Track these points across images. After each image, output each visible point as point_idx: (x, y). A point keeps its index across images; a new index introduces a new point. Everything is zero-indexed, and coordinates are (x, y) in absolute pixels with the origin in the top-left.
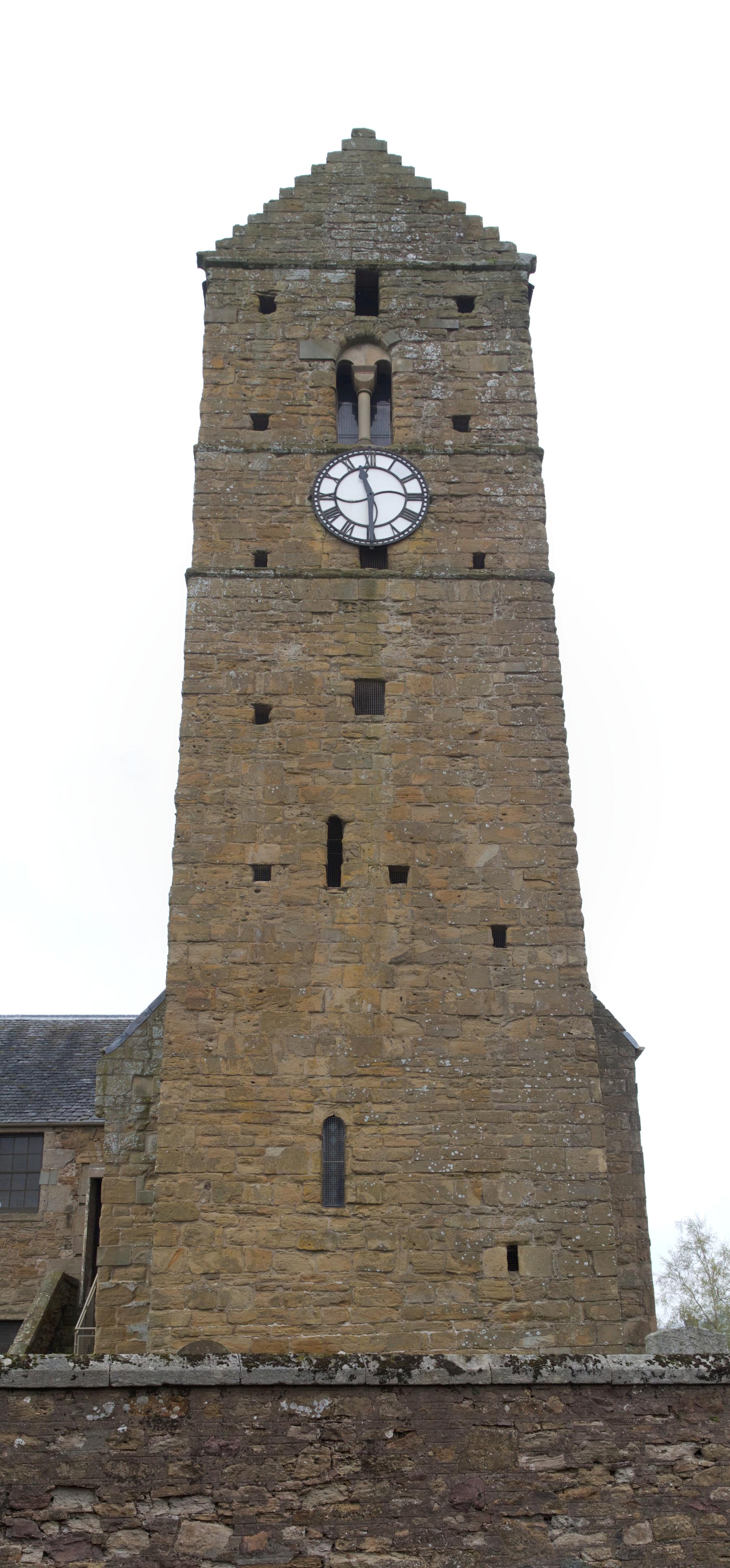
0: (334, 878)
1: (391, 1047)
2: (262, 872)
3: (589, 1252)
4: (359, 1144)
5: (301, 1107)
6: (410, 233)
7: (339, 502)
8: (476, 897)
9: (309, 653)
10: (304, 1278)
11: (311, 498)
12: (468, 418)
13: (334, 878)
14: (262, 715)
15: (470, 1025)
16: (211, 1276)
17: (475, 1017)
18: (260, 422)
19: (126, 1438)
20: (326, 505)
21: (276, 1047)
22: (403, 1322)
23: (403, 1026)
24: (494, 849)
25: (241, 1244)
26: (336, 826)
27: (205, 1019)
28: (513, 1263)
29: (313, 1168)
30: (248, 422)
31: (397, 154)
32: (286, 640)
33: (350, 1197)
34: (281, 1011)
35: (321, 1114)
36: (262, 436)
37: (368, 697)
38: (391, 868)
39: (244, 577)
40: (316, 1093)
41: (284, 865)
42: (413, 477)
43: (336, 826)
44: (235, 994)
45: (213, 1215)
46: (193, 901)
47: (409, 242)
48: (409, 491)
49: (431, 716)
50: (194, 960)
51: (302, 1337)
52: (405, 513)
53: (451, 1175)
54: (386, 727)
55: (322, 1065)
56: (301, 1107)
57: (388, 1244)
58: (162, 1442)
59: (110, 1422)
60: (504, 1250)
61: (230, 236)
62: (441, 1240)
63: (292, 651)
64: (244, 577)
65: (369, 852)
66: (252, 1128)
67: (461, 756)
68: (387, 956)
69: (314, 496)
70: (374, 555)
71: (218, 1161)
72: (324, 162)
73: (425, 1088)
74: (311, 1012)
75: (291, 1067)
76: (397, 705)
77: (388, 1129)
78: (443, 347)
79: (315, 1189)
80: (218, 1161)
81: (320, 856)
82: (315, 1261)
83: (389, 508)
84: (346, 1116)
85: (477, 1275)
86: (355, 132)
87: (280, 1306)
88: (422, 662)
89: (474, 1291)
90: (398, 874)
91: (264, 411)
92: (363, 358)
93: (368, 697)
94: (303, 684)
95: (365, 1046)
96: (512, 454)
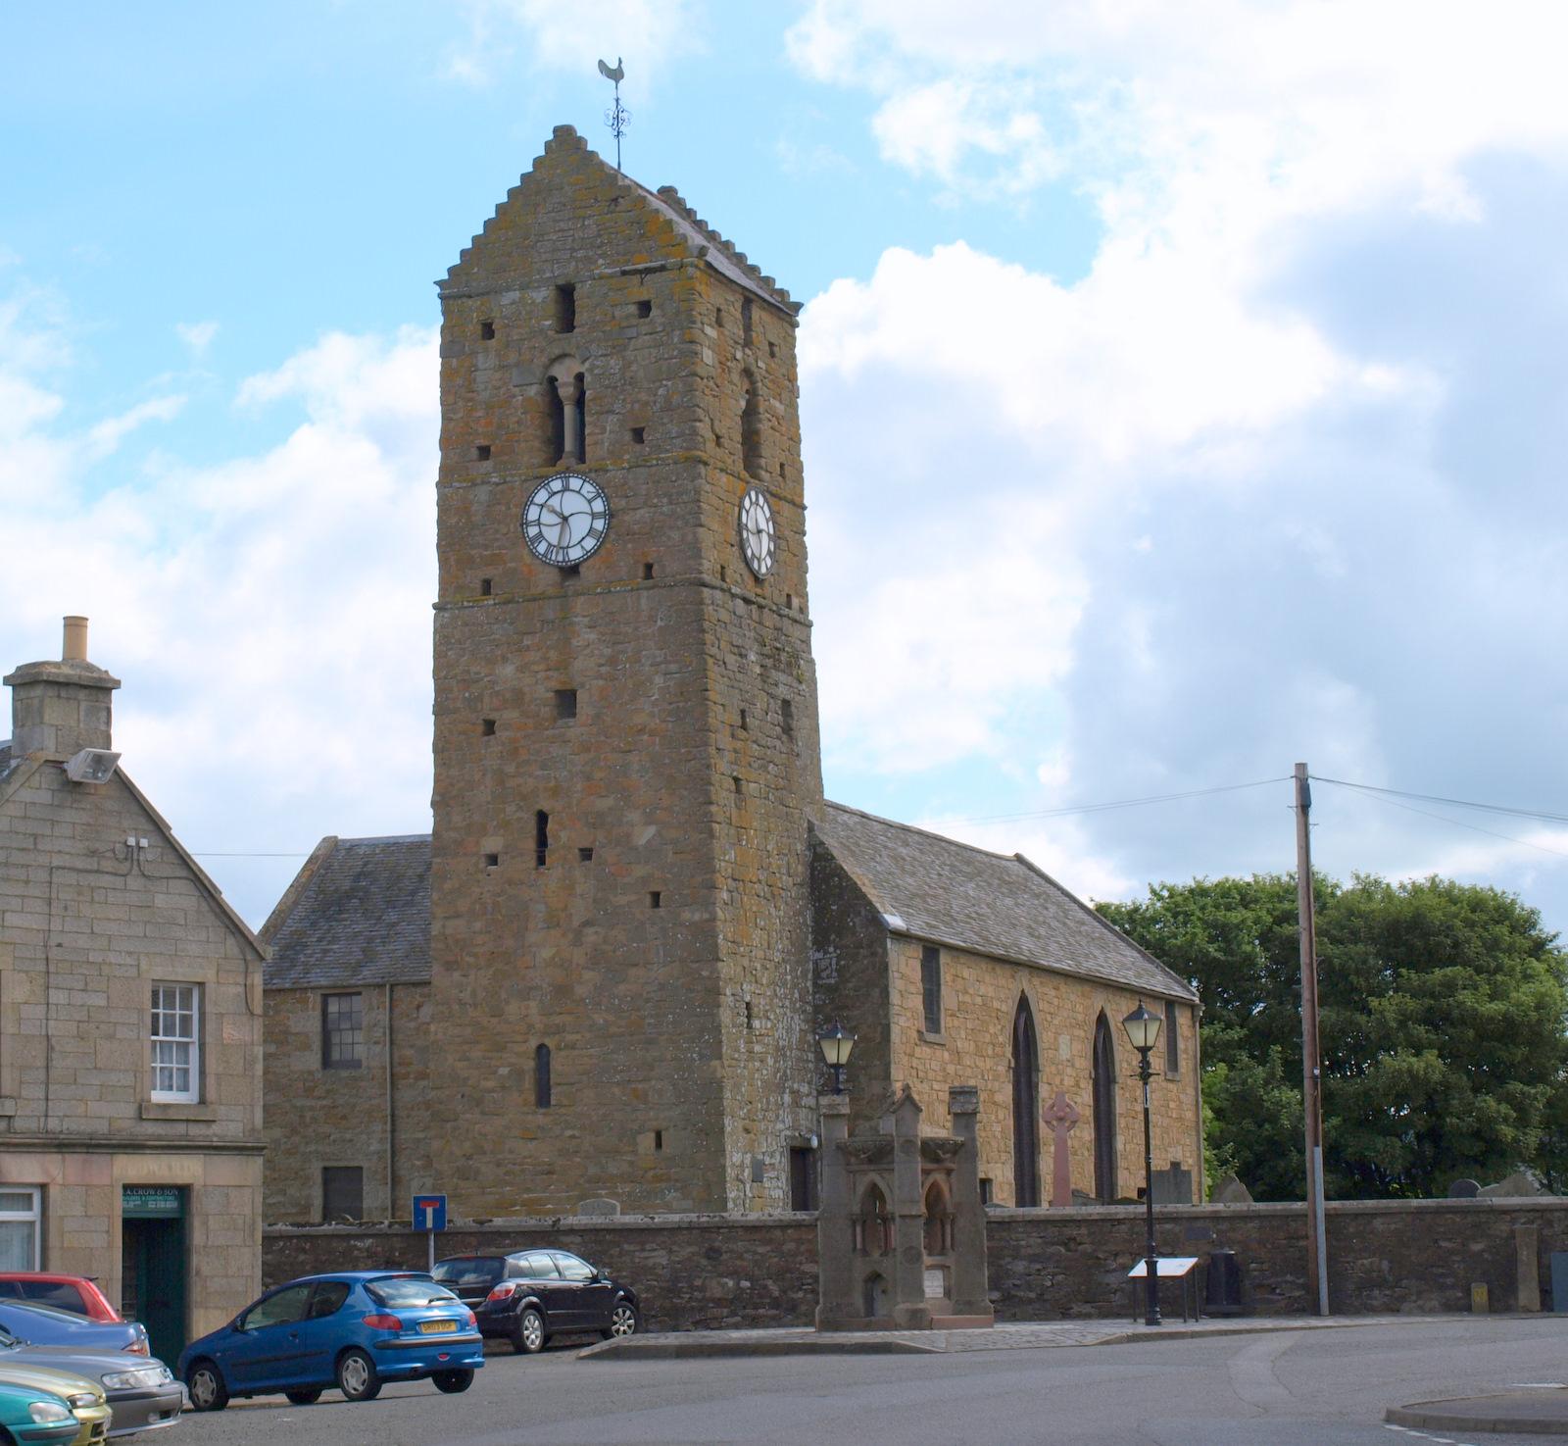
0: (541, 861)
1: (580, 991)
2: (493, 859)
3: (707, 1134)
4: (557, 1064)
5: (519, 1038)
6: (600, 236)
7: (543, 528)
8: (639, 871)
9: (521, 669)
10: (525, 1157)
11: (522, 525)
12: (643, 429)
13: (541, 861)
14: (490, 727)
15: (633, 971)
16: (469, 1157)
17: (636, 965)
18: (485, 452)
19: (289, 1255)
20: (533, 531)
21: (504, 996)
22: (587, 1185)
23: (588, 975)
24: (652, 830)
25: (486, 1135)
26: (542, 818)
27: (456, 975)
28: (659, 1144)
29: (529, 1083)
30: (474, 453)
31: (494, 209)
32: (505, 659)
33: (553, 1102)
34: (506, 968)
35: (533, 1043)
36: (488, 465)
37: (567, 701)
38: (581, 850)
39: (472, 607)
40: (531, 1026)
41: (506, 853)
42: (599, 495)
43: (542, 818)
44: (475, 955)
45: (468, 1116)
46: (445, 886)
47: (599, 247)
48: (595, 510)
49: (609, 719)
50: (448, 931)
51: (525, 1196)
52: (591, 531)
53: (618, 1084)
54: (577, 729)
55: (533, 1007)
56: (519, 1038)
57: (576, 1133)
58: (302, 1257)
59: (282, 1250)
60: (653, 1135)
61: (459, 262)
62: (611, 1129)
63: (508, 670)
64: (472, 607)
65: (562, 836)
66: (490, 1055)
67: (630, 751)
68: (576, 923)
69: (524, 524)
70: (571, 570)
71: (468, 1078)
72: (531, 169)
73: (601, 1021)
74: (527, 968)
75: (513, 1009)
76: (501, 734)
77: (576, 1052)
78: (624, 358)
79: (532, 1098)
80: (468, 1078)
81: (531, 845)
82: (532, 1145)
83: (580, 526)
84: (550, 1042)
85: (635, 1152)
86: (556, 130)
87: (1212, 1198)
88: (603, 669)
89: (631, 1163)
90: (587, 854)
91: (486, 443)
92: (565, 373)
93: (567, 701)
94: (518, 698)
95: (562, 991)
96: (675, 463)
